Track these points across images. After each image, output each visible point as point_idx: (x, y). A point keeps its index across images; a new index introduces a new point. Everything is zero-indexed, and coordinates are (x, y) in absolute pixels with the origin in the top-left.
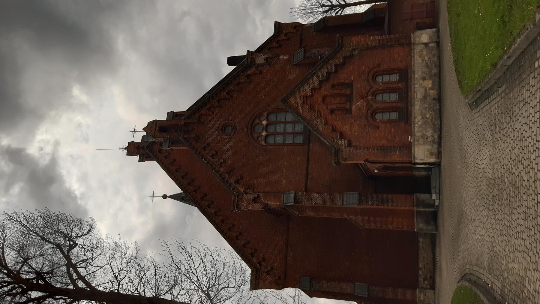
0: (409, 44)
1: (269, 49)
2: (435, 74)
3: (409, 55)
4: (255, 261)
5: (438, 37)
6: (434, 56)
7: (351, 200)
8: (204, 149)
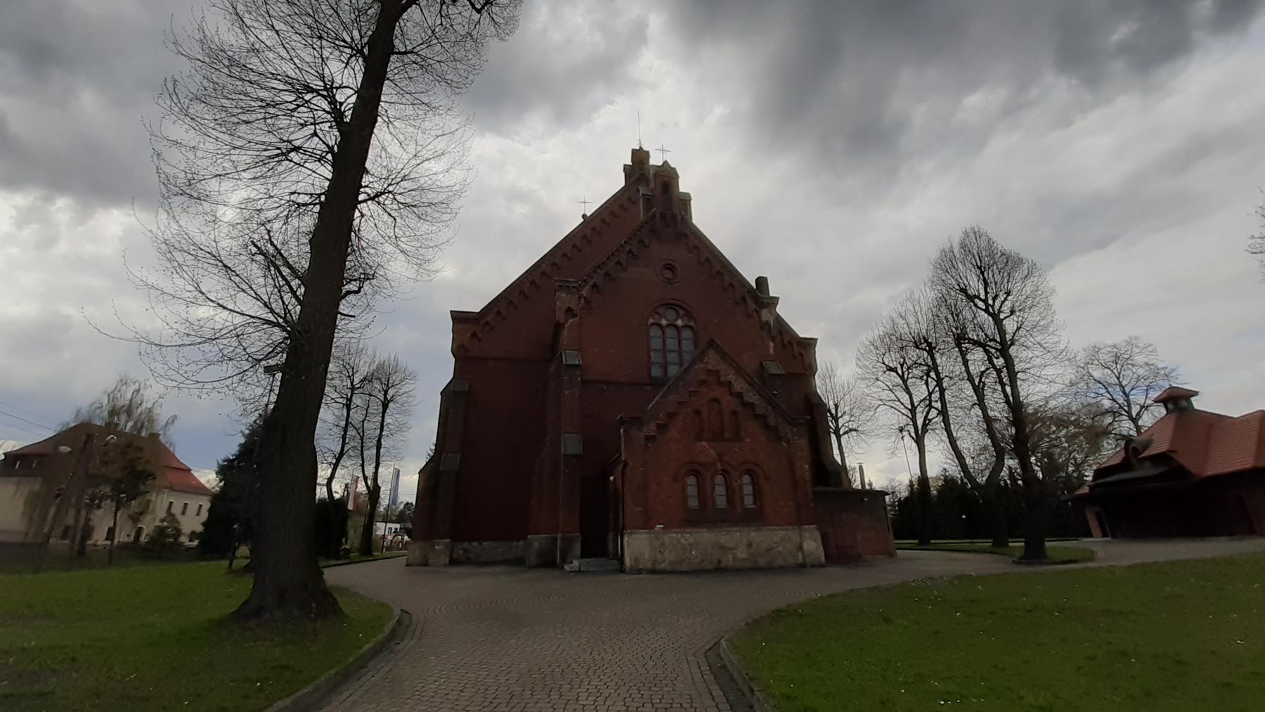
4: (489, 318)
5: (812, 566)
7: (571, 444)
8: (641, 241)
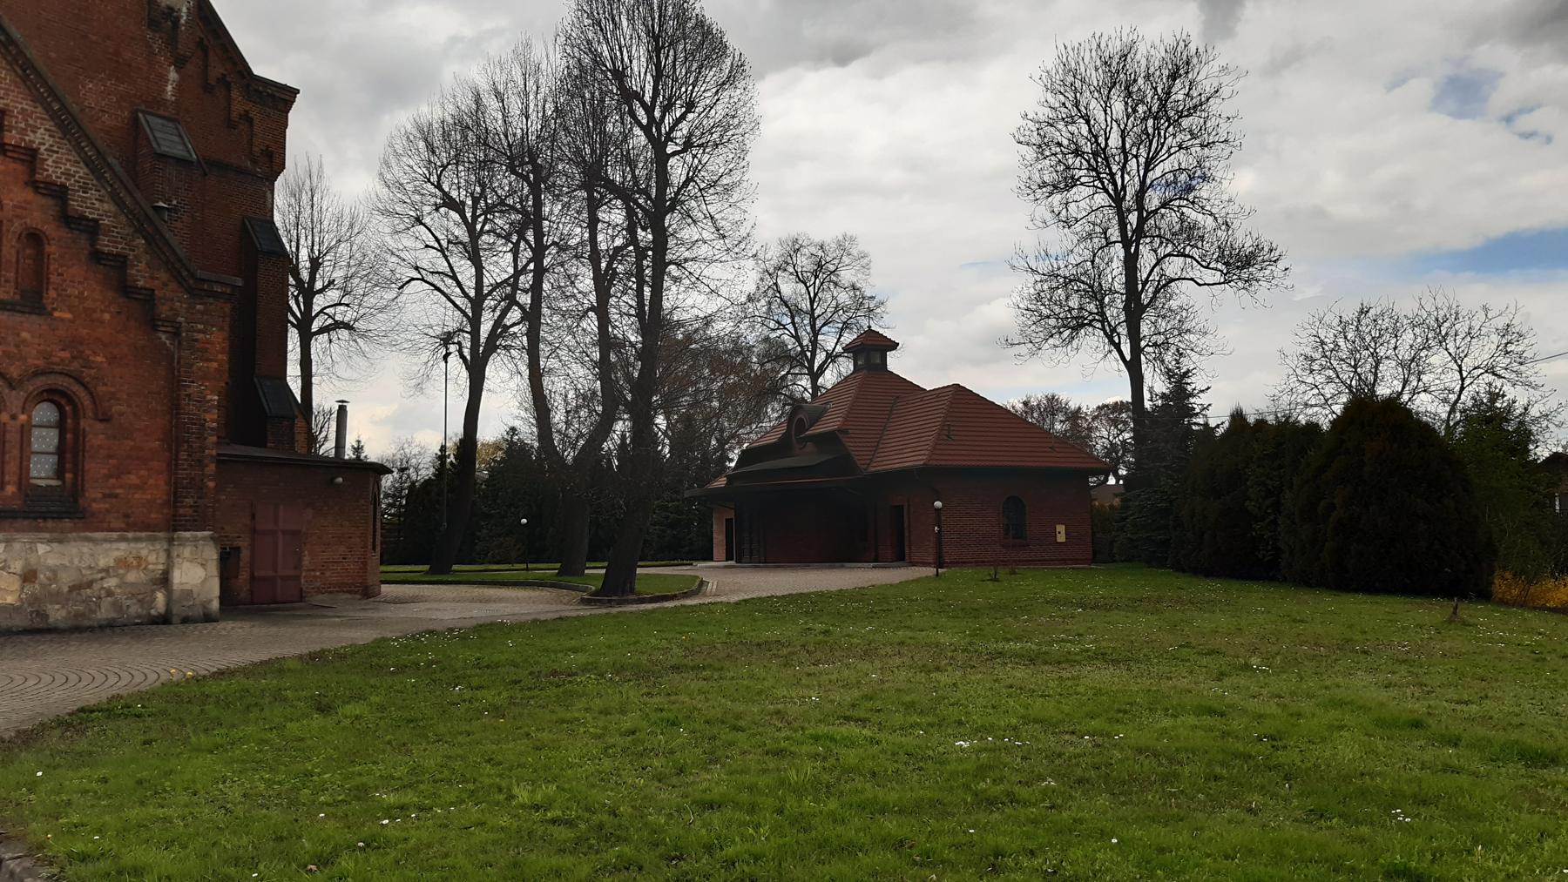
0: (172, 522)
1: (200, 43)
2: (43, 615)
3: (133, 524)
5: (186, 620)
6: (117, 606)
